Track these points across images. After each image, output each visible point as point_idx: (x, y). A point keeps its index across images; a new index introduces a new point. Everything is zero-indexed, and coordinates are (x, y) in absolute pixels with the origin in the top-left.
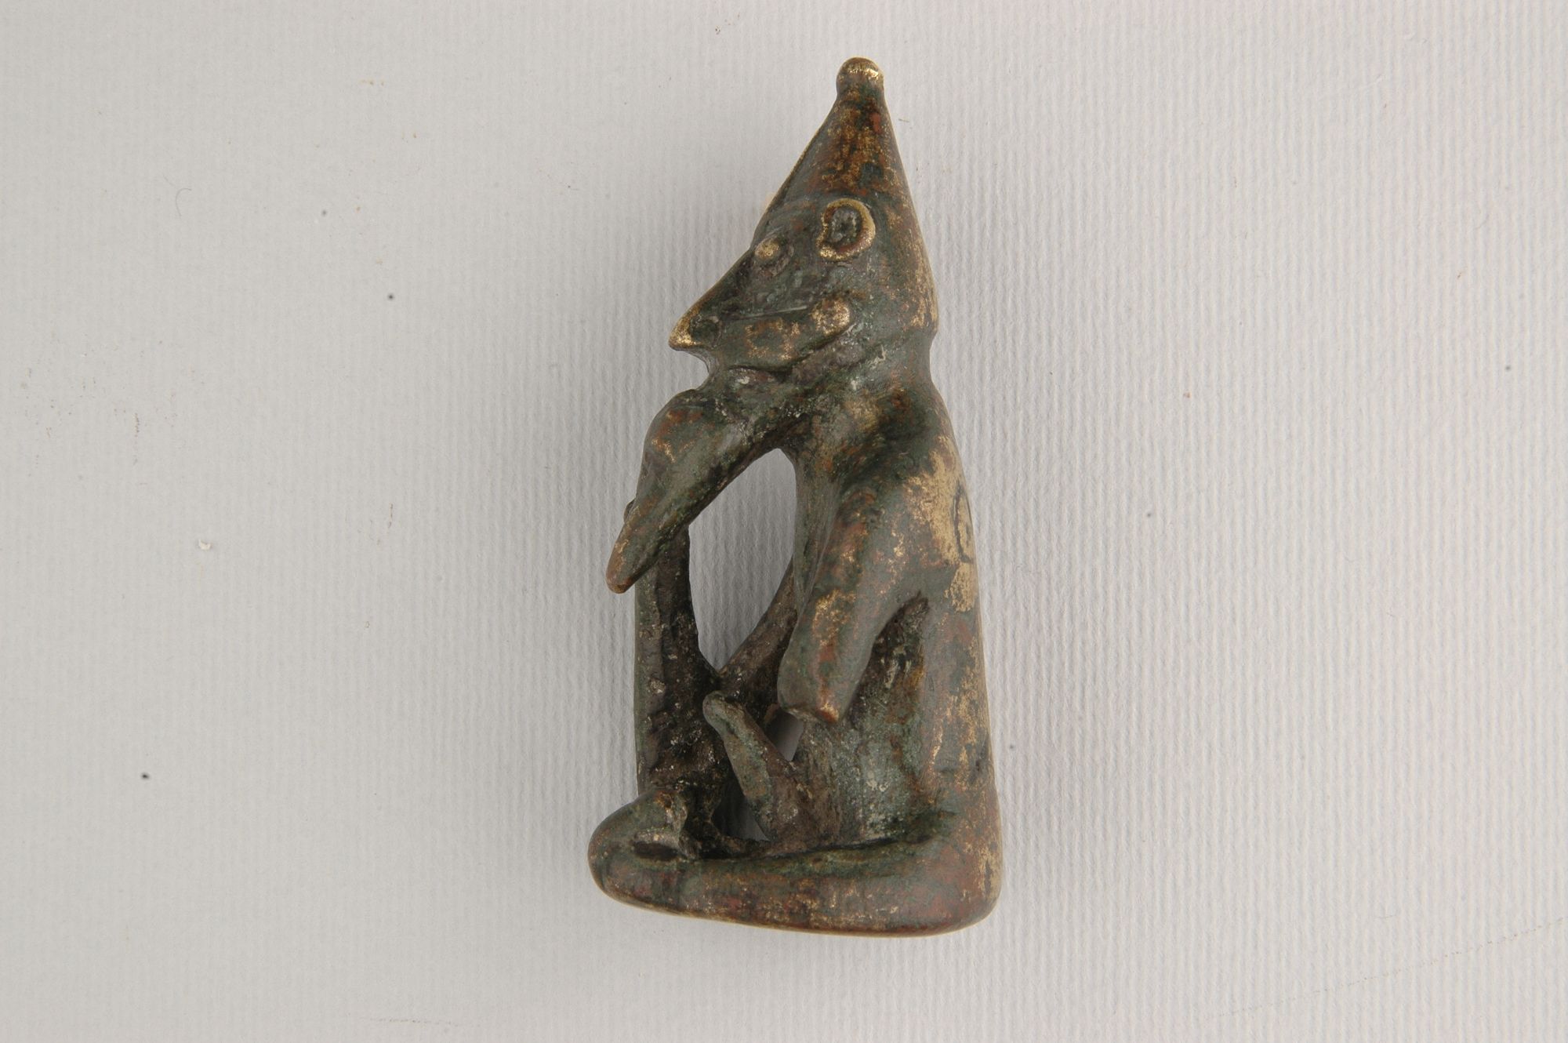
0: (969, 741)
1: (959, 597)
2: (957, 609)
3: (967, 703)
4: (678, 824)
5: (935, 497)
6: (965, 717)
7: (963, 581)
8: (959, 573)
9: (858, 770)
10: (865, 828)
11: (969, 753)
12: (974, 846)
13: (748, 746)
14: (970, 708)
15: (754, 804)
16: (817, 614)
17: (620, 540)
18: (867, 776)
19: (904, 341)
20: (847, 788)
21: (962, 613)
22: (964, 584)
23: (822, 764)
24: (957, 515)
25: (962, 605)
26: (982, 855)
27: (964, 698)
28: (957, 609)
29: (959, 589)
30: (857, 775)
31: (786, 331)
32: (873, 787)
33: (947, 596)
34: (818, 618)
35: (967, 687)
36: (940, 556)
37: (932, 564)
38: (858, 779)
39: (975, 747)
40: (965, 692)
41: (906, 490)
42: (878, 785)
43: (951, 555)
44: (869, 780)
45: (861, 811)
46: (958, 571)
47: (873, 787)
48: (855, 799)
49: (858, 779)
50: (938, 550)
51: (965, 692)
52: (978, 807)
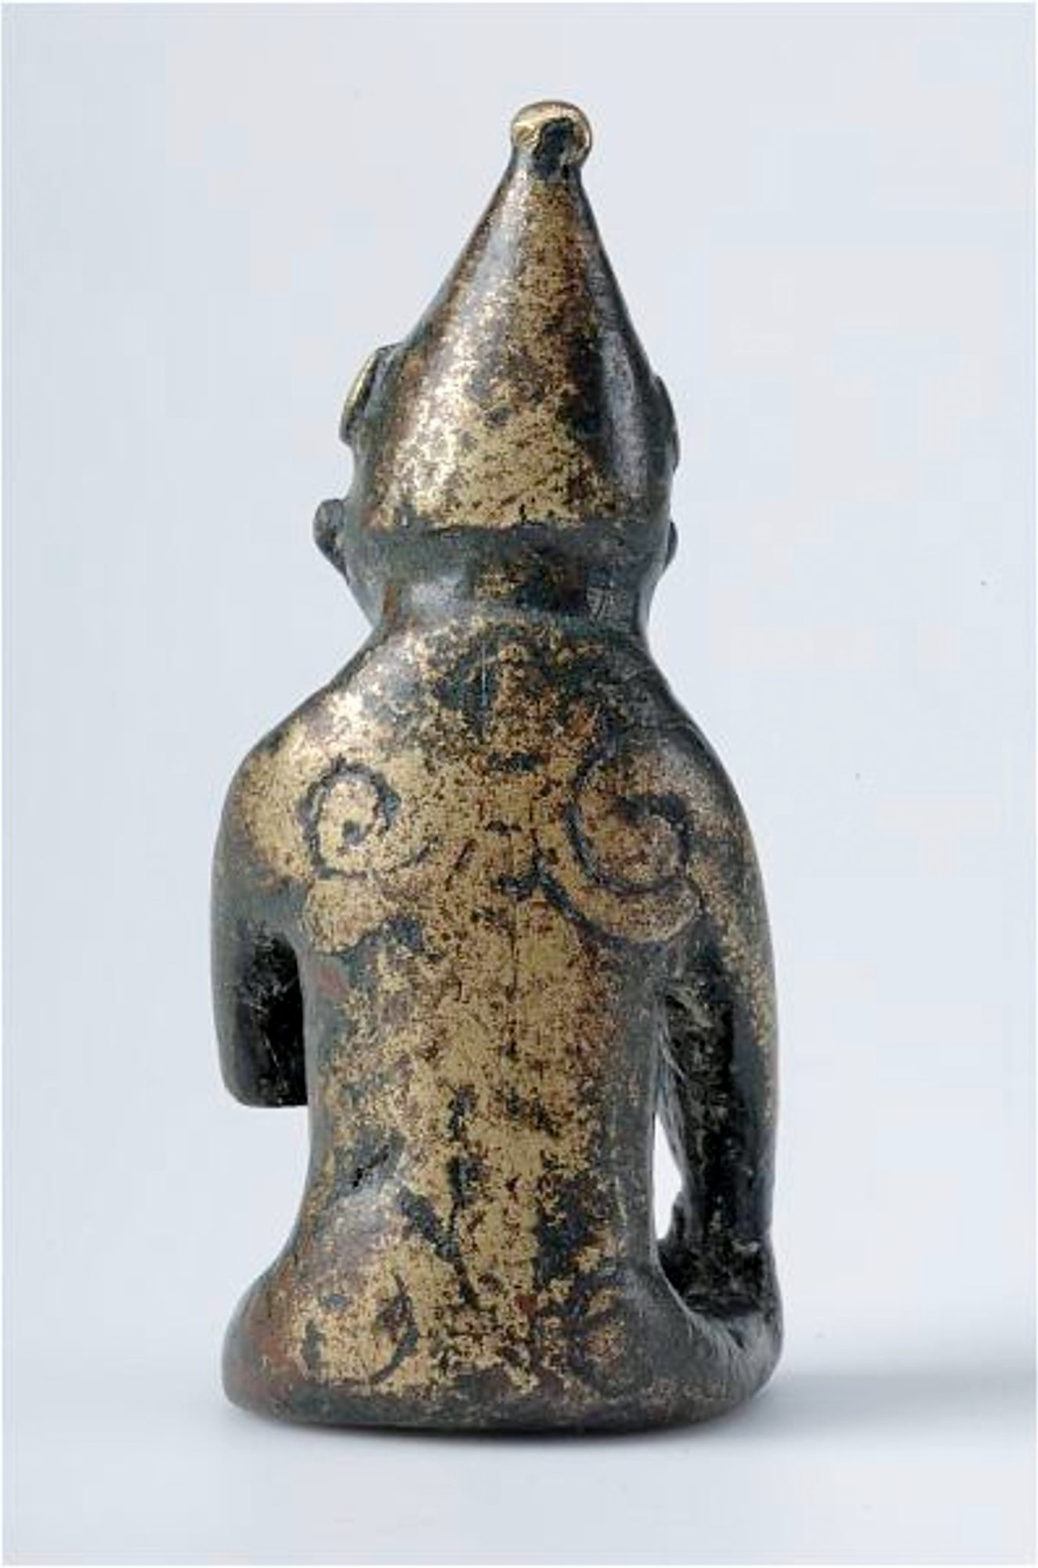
0: (340, 1143)
1: (318, 931)
2: (317, 948)
3: (339, 1087)
4: (476, 1033)
5: (263, 788)
6: (334, 1107)
7: (321, 906)
8: (314, 897)
11: (338, 1162)
12: (290, 1295)
14: (341, 1094)
21: (324, 954)
22: (326, 911)
24: (321, 809)
25: (325, 943)
26: (301, 1311)
27: (333, 1079)
28: (317, 948)
29: (317, 920)
33: (301, 929)
35: (338, 1063)
36: (273, 872)
37: (262, 884)
39: (349, 1151)
40: (335, 1070)
41: (383, 688)
43: (299, 868)
46: (312, 892)
50: (266, 862)
51: (335, 1070)
52: (320, 1240)
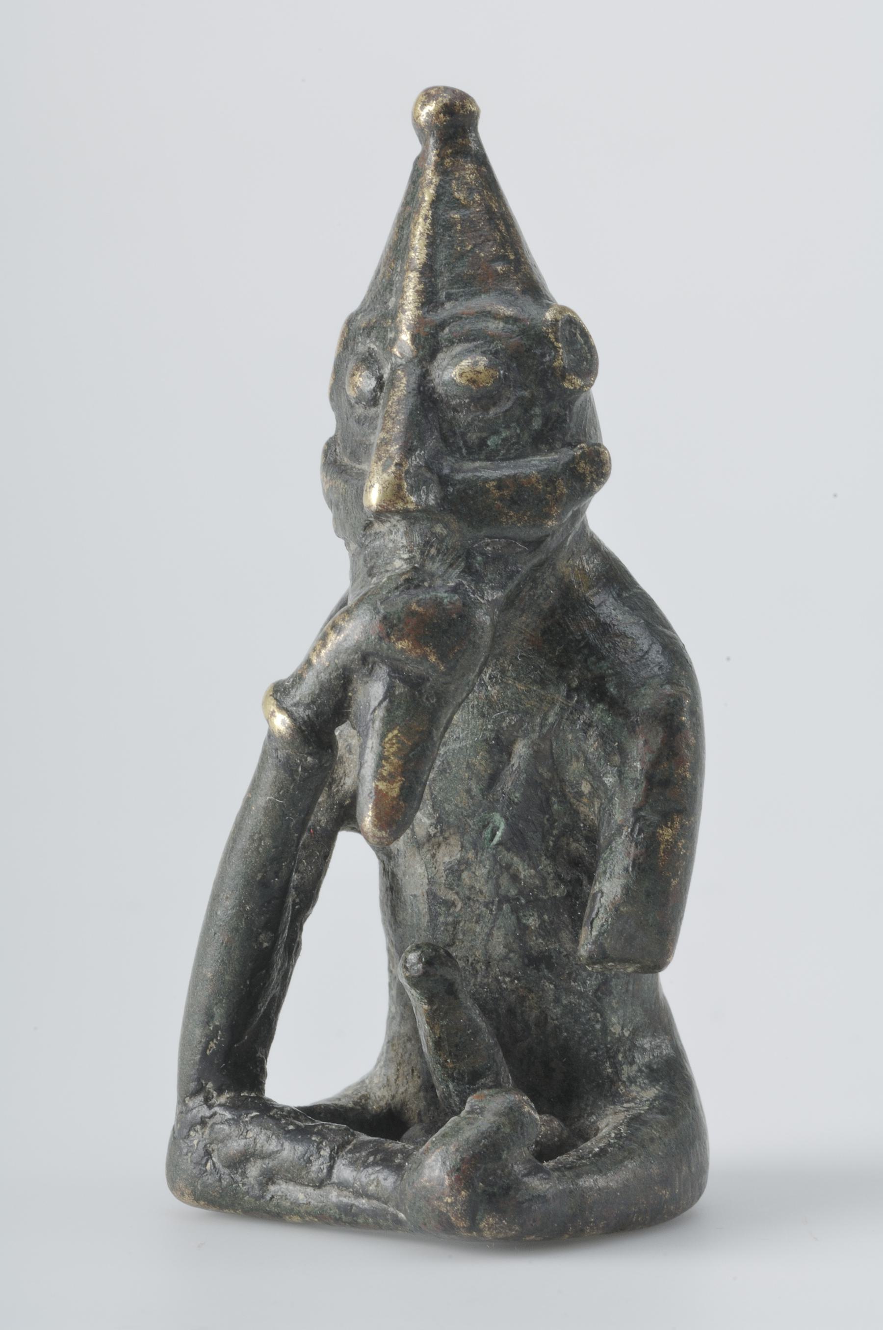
9: (598, 1015)
10: (626, 1087)
13: (410, 721)
15: (568, 438)
16: (662, 847)
17: (428, 922)
18: (610, 1020)
19: (345, 775)
20: (580, 1038)
23: (522, 1012)
30: (598, 1022)
31: (549, 489)
32: (617, 1033)
34: (663, 852)
38: (598, 1026)
42: (622, 1029)
44: (613, 1025)
45: (608, 1064)
47: (617, 1033)
48: (597, 1051)
49: (598, 1026)
